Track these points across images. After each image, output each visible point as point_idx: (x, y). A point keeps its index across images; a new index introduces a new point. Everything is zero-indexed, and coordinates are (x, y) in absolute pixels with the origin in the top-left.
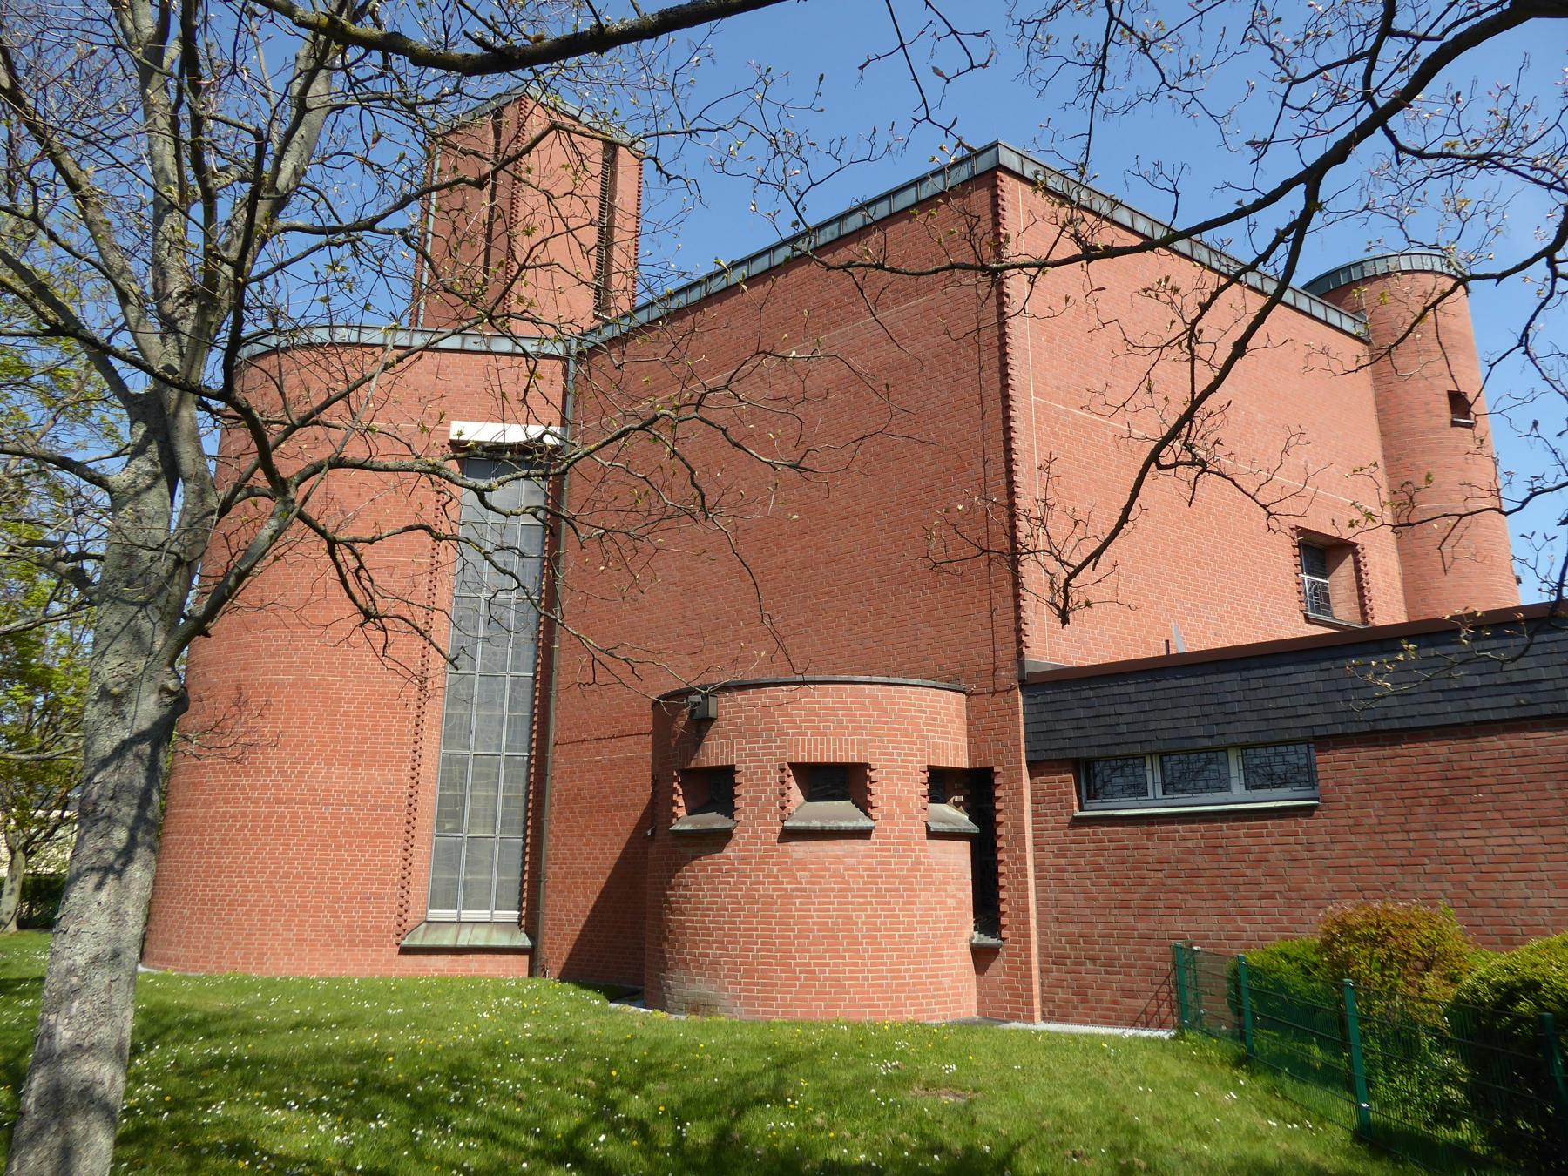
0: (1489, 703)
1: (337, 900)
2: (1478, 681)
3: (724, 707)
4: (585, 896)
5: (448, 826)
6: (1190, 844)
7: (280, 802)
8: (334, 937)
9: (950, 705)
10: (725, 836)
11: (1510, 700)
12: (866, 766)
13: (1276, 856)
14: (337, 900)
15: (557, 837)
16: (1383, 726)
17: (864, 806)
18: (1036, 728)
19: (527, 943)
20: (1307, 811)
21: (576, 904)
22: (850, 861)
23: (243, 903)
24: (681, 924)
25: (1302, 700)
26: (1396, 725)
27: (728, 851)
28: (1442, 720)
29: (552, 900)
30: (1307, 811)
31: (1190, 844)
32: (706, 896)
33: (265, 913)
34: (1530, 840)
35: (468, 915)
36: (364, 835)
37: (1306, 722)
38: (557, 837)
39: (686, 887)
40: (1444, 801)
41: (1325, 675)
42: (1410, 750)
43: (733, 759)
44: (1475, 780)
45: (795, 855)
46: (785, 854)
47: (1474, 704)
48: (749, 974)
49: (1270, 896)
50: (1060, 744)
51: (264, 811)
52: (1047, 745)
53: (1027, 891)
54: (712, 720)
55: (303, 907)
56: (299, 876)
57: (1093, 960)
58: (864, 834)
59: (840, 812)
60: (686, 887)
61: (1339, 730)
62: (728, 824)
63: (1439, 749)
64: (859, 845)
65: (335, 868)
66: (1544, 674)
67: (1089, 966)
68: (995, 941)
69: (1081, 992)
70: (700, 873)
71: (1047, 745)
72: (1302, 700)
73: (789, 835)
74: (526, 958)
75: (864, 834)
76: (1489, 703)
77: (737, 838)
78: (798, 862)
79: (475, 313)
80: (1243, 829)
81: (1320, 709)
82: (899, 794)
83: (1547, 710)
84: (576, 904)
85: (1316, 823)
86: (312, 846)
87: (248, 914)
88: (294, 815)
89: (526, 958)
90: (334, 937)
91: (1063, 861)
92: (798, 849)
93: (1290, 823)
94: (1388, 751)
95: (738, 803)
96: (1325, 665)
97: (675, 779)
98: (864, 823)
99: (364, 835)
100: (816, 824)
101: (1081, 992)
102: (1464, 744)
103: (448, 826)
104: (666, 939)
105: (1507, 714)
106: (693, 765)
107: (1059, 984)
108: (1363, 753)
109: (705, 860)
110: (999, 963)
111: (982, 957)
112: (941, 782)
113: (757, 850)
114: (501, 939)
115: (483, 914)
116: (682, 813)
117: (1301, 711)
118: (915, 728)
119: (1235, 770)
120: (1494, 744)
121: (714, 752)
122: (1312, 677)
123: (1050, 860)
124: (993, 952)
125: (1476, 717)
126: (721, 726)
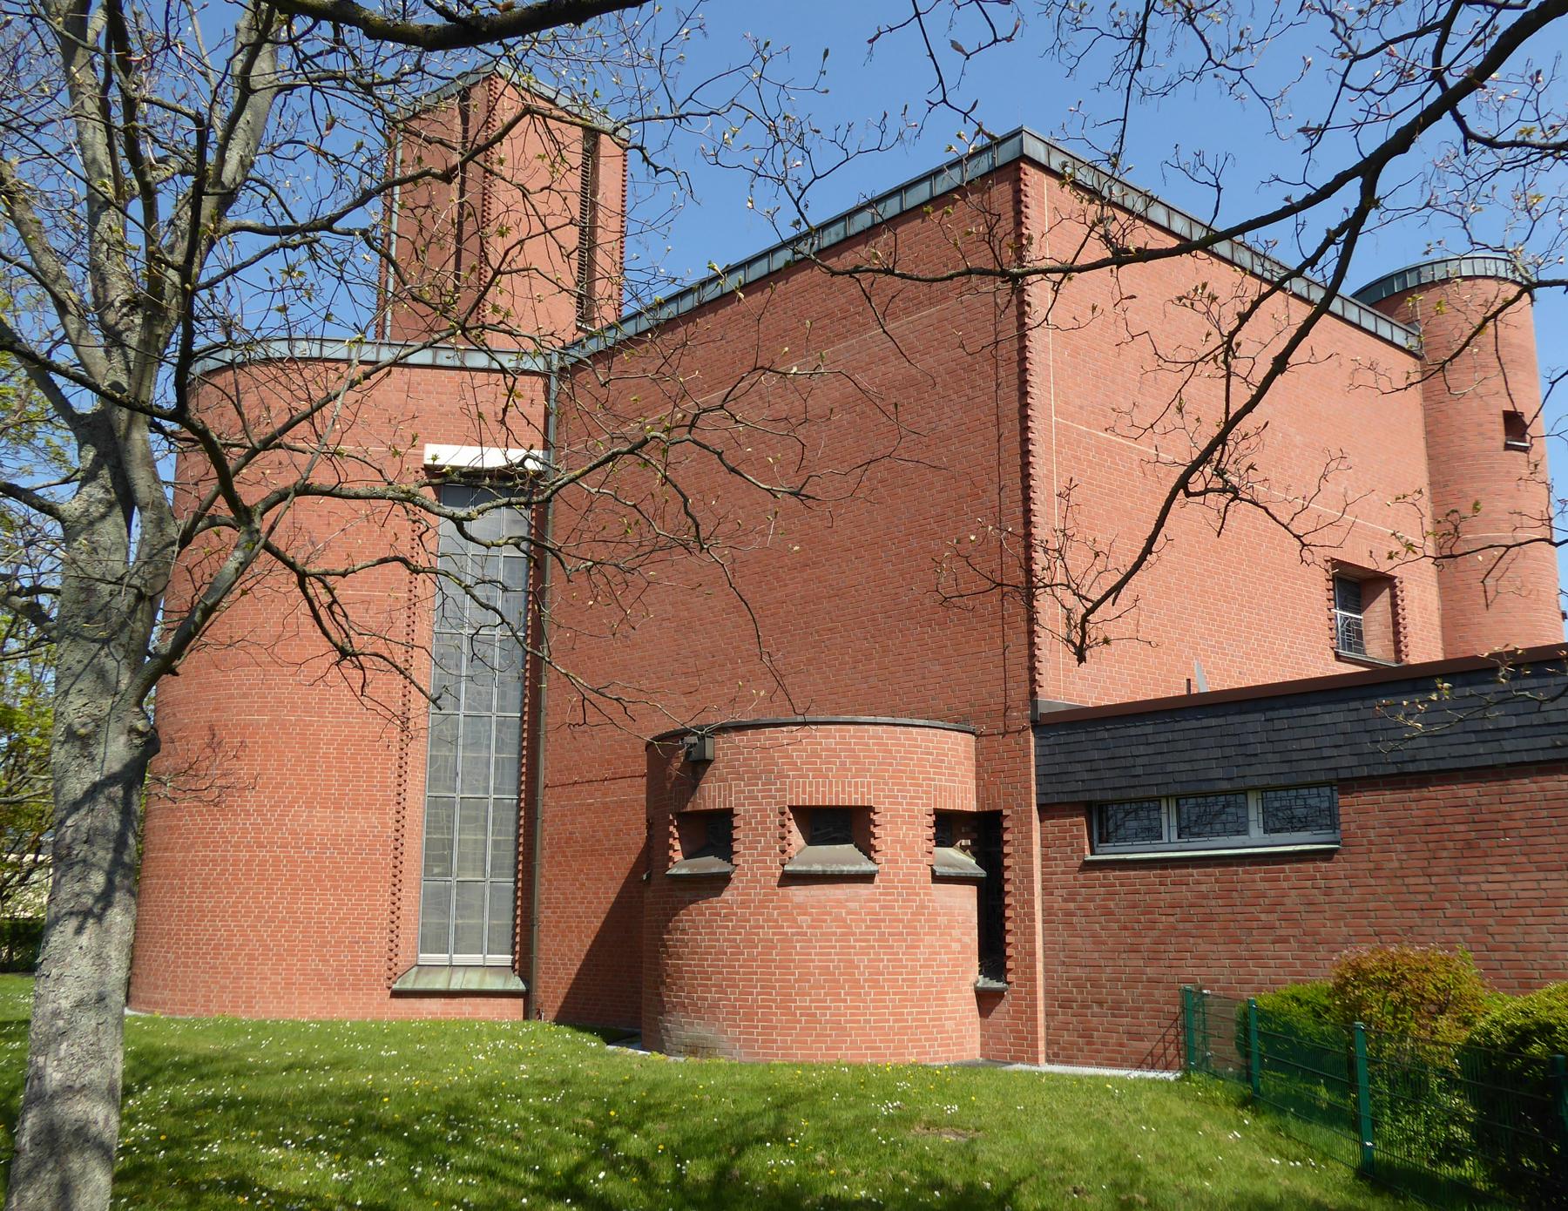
0: (1524, 744)
3: (721, 748)
4: (580, 940)
5: (436, 870)
6: (1203, 888)
8: (322, 979)
10: (722, 881)
11: (1545, 742)
12: (870, 809)
14: (324, 944)
16: (1411, 768)
17: (867, 850)
19: (522, 987)
20: (1327, 855)
23: (229, 948)
24: (678, 969)
25: (1328, 741)
26: (1425, 767)
27: (727, 895)
28: (1473, 762)
29: (545, 945)
30: (1327, 855)
31: (1203, 888)
32: (704, 939)
33: (251, 957)
35: (459, 959)
36: (349, 879)
39: (683, 931)
40: (1469, 845)
41: (1353, 716)
43: (732, 802)
44: (1504, 823)
45: (796, 900)
46: (786, 898)
48: (749, 1017)
49: (1284, 940)
51: (244, 855)
52: (1059, 788)
53: (1034, 935)
54: (709, 762)
55: (291, 952)
56: (284, 921)
57: (1100, 1004)
58: (867, 878)
60: (683, 931)
61: (1365, 772)
62: (726, 868)
63: (1468, 792)
64: (862, 889)
65: (321, 912)
67: (1096, 1009)
69: (1087, 1034)
71: (1059, 788)
72: (1328, 741)
73: (789, 879)
74: (520, 1002)
75: (867, 878)
76: (1524, 744)
77: (735, 883)
80: (1259, 873)
81: (1347, 750)
82: (904, 838)
85: (1337, 867)
86: (296, 890)
87: (234, 958)
88: (277, 859)
89: (520, 1002)
90: (322, 979)
91: (1072, 905)
92: (798, 893)
94: (1414, 794)
96: (1353, 705)
97: (671, 822)
98: (868, 867)
100: (817, 868)
101: (1087, 1034)
102: (1495, 787)
103: (436, 870)
104: (663, 983)
105: (1541, 756)
106: (689, 808)
107: (1065, 1026)
108: (1388, 796)
109: (703, 905)
110: (1003, 1006)
111: (986, 1001)
113: (757, 894)
115: (476, 958)
116: (678, 857)
117: (1327, 752)
118: (921, 769)
119: (1254, 813)
120: (1527, 787)
121: (711, 795)
122: (1340, 717)
123: (1058, 904)
124: (998, 995)
125: (1509, 759)
126: (719, 768)
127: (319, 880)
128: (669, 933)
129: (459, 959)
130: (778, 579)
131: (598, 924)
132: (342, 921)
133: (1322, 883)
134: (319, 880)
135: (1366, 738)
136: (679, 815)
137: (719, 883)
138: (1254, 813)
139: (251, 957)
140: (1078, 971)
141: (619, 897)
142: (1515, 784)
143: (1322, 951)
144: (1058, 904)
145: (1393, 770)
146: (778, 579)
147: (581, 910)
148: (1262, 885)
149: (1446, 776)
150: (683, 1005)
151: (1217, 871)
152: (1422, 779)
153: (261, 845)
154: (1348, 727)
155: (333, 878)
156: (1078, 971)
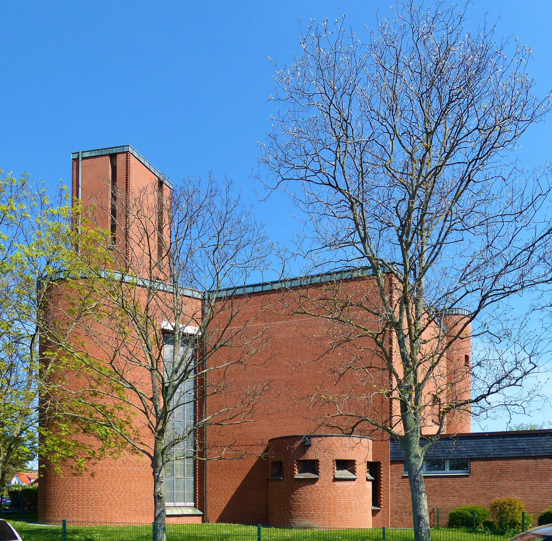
0: (514, 452)
1: (137, 500)
2: (512, 447)
3: (314, 441)
4: (225, 497)
5: (168, 474)
6: (435, 483)
7: (111, 465)
8: (137, 512)
9: (367, 443)
10: (317, 480)
11: (518, 452)
12: (355, 461)
13: (458, 487)
14: (137, 500)
15: (211, 479)
16: (488, 456)
17: (353, 472)
18: (393, 451)
19: (201, 513)
20: (467, 476)
21: (221, 500)
22: (351, 487)
23: (102, 501)
24: (299, 506)
25: (469, 449)
26: (491, 456)
27: (317, 484)
28: (502, 456)
29: (210, 499)
30: (467, 476)
31: (435, 483)
32: (309, 497)
33: (111, 505)
34: (517, 484)
35: (177, 504)
36: (144, 477)
37: (470, 454)
38: (211, 479)
39: (300, 494)
40: (499, 474)
41: (476, 443)
42: (493, 462)
43: (318, 457)
44: (508, 470)
45: (338, 486)
46: (334, 485)
47: (510, 453)
48: (324, 518)
49: (455, 496)
50: (401, 456)
51: (105, 468)
52: (397, 456)
53: (386, 495)
54: (310, 445)
55: (125, 502)
56: (122, 492)
57: (406, 513)
58: (354, 480)
59: (345, 473)
60: (300, 494)
61: (478, 457)
62: (317, 477)
63: (500, 462)
64: (353, 483)
65: (134, 489)
66: (527, 447)
67: (404, 514)
68: (378, 508)
69: (402, 520)
70: (305, 492)
71: (397, 456)
72: (469, 449)
73: (335, 480)
74: (201, 518)
75: (354, 480)
76: (514, 452)
77: (319, 480)
78: (338, 487)
79: (147, 283)
80: (450, 480)
81: (473, 451)
82: (362, 470)
83: (526, 455)
84: (221, 500)
85: (469, 479)
86: (126, 481)
87: (104, 505)
88: (118, 470)
89: (201, 518)
90: (137, 512)
91: (399, 487)
92: (338, 484)
93: (462, 479)
94: (488, 462)
95: (320, 470)
96: (476, 440)
97: (294, 463)
98: (354, 477)
99: (144, 477)
100: (343, 477)
101: (402, 520)
102: (506, 462)
103: (168, 474)
104: (291, 509)
105: (517, 455)
106: (302, 459)
107: (396, 519)
108: (482, 462)
109: (308, 487)
110: (379, 514)
111: (374, 513)
112: (370, 464)
113: (326, 484)
114: (190, 511)
115: (183, 504)
116: (297, 473)
117: (469, 451)
118: (362, 450)
119: (447, 465)
120: (513, 462)
121: (310, 455)
122: (472, 443)
123: (395, 487)
124: (378, 511)
125: (510, 456)
126: (313, 447)
127: (133, 478)
128: (294, 495)
129: (177, 504)
130: (304, 387)
131: (233, 492)
132: (142, 492)
133: (465, 483)
134: (133, 478)
135: (479, 448)
136: (299, 462)
137: (314, 481)
138: (447, 465)
139: (111, 505)
140: (400, 505)
141: (242, 483)
142: (511, 461)
143: (464, 499)
144: (395, 487)
145: (484, 457)
146: (304, 387)
147: (225, 488)
148: (450, 483)
149: (495, 459)
150: (301, 515)
151: (439, 479)
152: (491, 459)
153: (111, 465)
154: (474, 446)
155: (138, 477)
156: (400, 505)
